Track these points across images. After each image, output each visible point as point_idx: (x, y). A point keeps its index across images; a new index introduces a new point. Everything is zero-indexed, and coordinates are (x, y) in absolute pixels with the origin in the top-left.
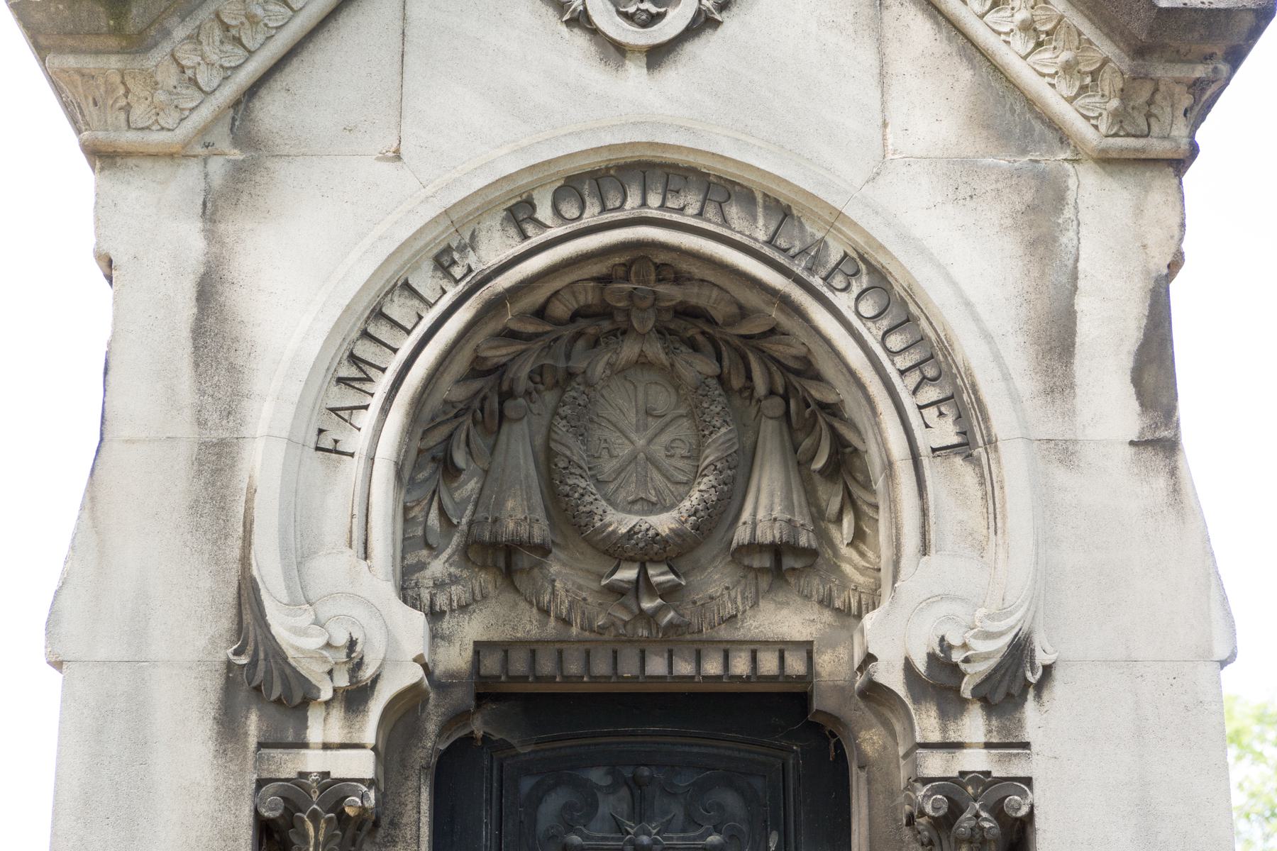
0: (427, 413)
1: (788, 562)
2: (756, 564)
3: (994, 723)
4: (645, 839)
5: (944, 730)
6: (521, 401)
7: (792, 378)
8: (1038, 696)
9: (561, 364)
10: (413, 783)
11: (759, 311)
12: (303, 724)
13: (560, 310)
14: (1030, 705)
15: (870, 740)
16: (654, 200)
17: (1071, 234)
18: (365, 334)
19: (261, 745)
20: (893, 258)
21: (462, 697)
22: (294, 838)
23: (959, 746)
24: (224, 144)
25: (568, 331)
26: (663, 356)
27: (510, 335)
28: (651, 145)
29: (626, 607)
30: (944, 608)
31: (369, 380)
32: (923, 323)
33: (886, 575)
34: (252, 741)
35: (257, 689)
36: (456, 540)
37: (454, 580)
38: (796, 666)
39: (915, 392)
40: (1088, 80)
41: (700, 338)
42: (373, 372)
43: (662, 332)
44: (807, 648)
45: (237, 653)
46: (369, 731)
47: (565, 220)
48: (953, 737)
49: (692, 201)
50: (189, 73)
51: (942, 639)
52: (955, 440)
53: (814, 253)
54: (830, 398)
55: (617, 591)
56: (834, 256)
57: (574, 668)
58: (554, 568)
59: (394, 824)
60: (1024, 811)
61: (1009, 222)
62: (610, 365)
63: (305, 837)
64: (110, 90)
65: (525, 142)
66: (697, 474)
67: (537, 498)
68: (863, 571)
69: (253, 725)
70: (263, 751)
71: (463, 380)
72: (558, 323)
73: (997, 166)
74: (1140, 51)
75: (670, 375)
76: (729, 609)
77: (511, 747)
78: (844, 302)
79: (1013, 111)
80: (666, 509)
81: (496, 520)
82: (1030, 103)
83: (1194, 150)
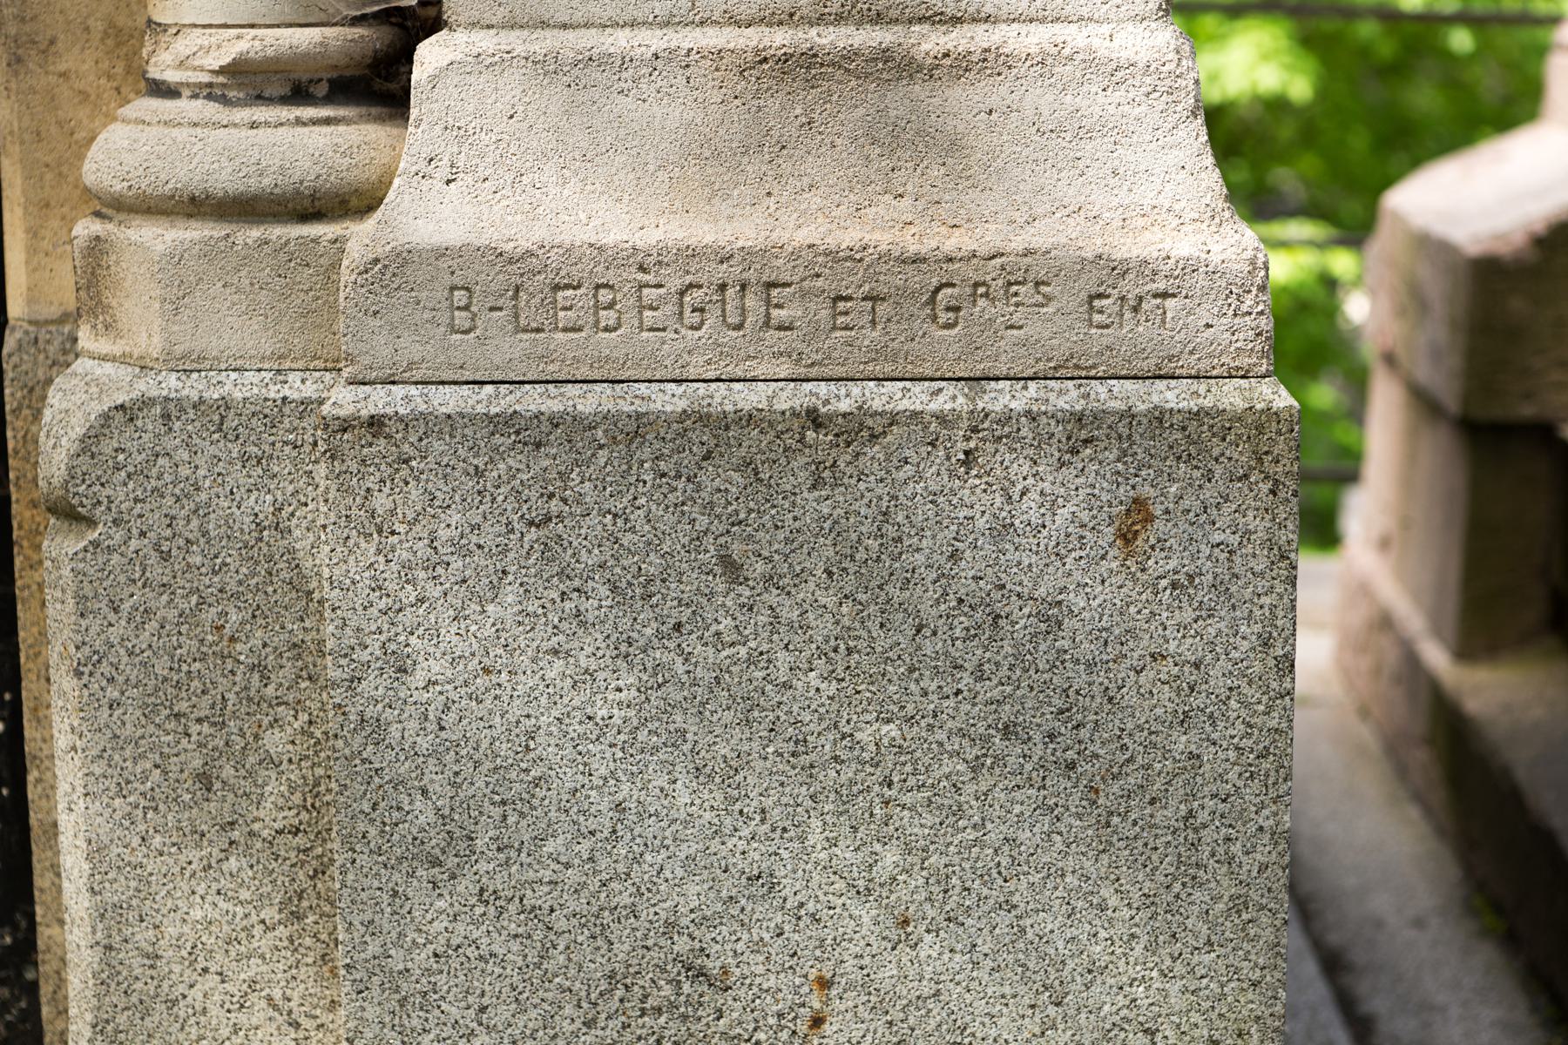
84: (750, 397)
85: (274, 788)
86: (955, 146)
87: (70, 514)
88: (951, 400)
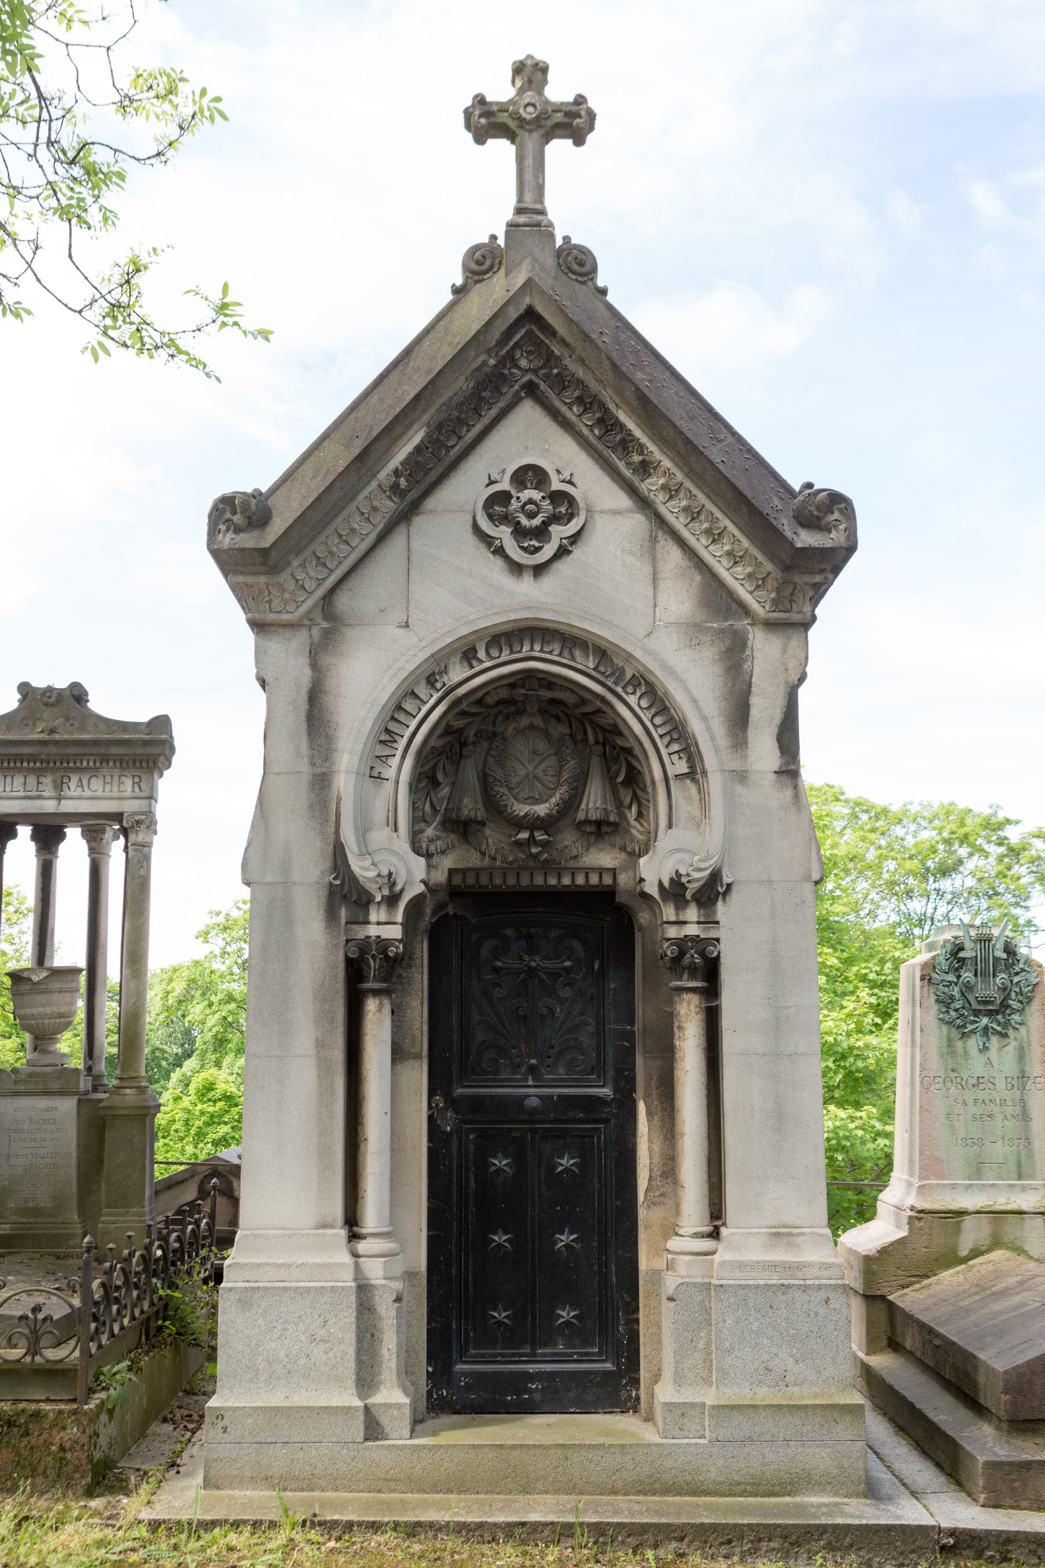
0: (424, 755)
1: (604, 829)
2: (588, 830)
3: (702, 911)
4: (533, 964)
5: (677, 915)
6: (471, 747)
7: (608, 735)
8: (724, 899)
9: (491, 729)
10: (419, 938)
11: (590, 701)
12: (367, 914)
13: (490, 700)
14: (720, 903)
15: (644, 917)
16: (537, 647)
17: (749, 663)
18: (393, 718)
19: (347, 923)
20: (658, 678)
21: (443, 896)
22: (364, 967)
23: (685, 923)
24: (319, 619)
25: (494, 711)
26: (542, 724)
27: (464, 714)
28: (535, 619)
29: (523, 852)
30: (679, 856)
31: (396, 741)
32: (672, 711)
33: (652, 835)
34: (343, 921)
35: (345, 896)
36: (439, 818)
37: (438, 838)
38: (608, 880)
39: (667, 746)
40: (760, 582)
41: (561, 714)
42: (397, 738)
43: (542, 712)
44: (613, 871)
45: (335, 879)
46: (399, 917)
47: (492, 658)
48: (682, 918)
49: (556, 647)
50: (301, 583)
51: (677, 871)
52: (686, 770)
53: (618, 674)
54: (627, 745)
55: (519, 844)
56: (628, 676)
57: (498, 881)
58: (488, 832)
59: (411, 958)
60: (715, 954)
61: (717, 657)
62: (515, 729)
63: (369, 966)
64: (261, 592)
65: (471, 617)
66: (559, 784)
67: (479, 798)
68: (641, 833)
69: (343, 913)
70: (349, 926)
71: (440, 736)
72: (489, 706)
73: (712, 628)
74: (787, 569)
75: (546, 734)
76: (575, 852)
77: (467, 919)
78: (632, 700)
79: (721, 598)
80: (543, 802)
81: (459, 809)
82: (730, 594)
83: (814, 618)
84: (773, 1282)
85: (702, 1342)
86: (799, 1246)
87: (671, 1299)
88: (801, 1282)
